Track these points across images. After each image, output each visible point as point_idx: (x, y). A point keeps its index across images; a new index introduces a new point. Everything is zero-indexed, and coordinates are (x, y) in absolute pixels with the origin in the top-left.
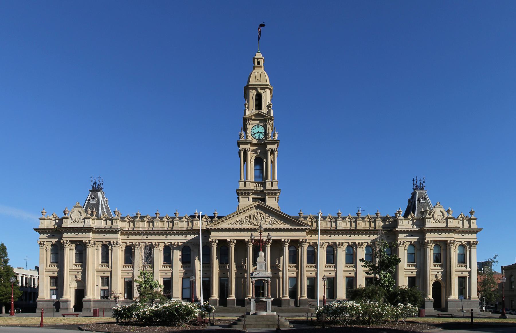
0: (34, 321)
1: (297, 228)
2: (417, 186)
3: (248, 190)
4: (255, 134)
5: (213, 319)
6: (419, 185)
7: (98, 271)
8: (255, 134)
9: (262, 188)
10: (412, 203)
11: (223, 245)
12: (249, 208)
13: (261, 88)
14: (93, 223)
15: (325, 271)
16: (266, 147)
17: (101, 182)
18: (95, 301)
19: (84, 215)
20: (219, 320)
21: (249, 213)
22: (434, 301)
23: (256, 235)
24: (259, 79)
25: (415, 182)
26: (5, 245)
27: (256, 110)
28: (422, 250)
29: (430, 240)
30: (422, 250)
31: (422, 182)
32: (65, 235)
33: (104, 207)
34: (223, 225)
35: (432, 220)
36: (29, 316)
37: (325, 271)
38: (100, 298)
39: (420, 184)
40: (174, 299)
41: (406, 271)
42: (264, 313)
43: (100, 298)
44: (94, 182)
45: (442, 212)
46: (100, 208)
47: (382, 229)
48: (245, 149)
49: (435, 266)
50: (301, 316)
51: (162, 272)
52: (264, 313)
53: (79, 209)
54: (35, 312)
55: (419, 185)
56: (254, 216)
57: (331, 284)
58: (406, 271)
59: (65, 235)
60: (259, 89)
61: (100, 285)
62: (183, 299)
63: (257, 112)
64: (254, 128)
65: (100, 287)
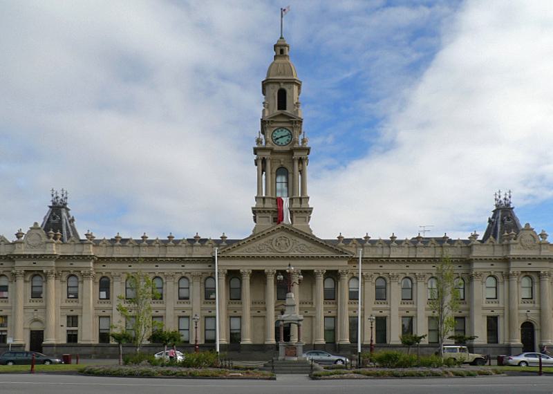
0: (395, 352)
1: (335, 255)
2: (500, 202)
3: (304, 208)
4: (277, 139)
5: (540, 356)
6: (503, 201)
7: (62, 308)
8: (277, 139)
9: (463, 335)
10: (493, 223)
11: (233, 275)
12: (260, 235)
13: (285, 83)
14: (55, 249)
15: (374, 309)
16: (293, 155)
17: (65, 196)
18: (58, 346)
19: (45, 239)
20: (55, 298)
21: (271, 237)
22: (523, 346)
23: (282, 265)
24: (283, 72)
25: (498, 197)
26: (313, 211)
27: (279, 109)
28: (506, 282)
29: (515, 271)
30: (506, 282)
31: (507, 197)
32: (18, 263)
33: (69, 227)
34: (235, 253)
35: (519, 246)
36: (201, 295)
37: (374, 309)
38: (64, 342)
39: (505, 199)
40: (285, 221)
41: (484, 308)
42: (295, 359)
43: (64, 342)
44: (55, 196)
45: (39, 235)
46: (64, 229)
47: (413, 335)
48: (264, 158)
49: (489, 303)
50: (504, 336)
51: (400, 309)
52: (295, 359)
53: (38, 232)
54: (77, 317)
55: (503, 201)
56: (276, 241)
57: (381, 324)
58: (484, 308)
59: (513, 264)
60: (282, 84)
61: (65, 325)
62: (231, 299)
63: (280, 112)
64: (276, 132)
65: (65, 328)
